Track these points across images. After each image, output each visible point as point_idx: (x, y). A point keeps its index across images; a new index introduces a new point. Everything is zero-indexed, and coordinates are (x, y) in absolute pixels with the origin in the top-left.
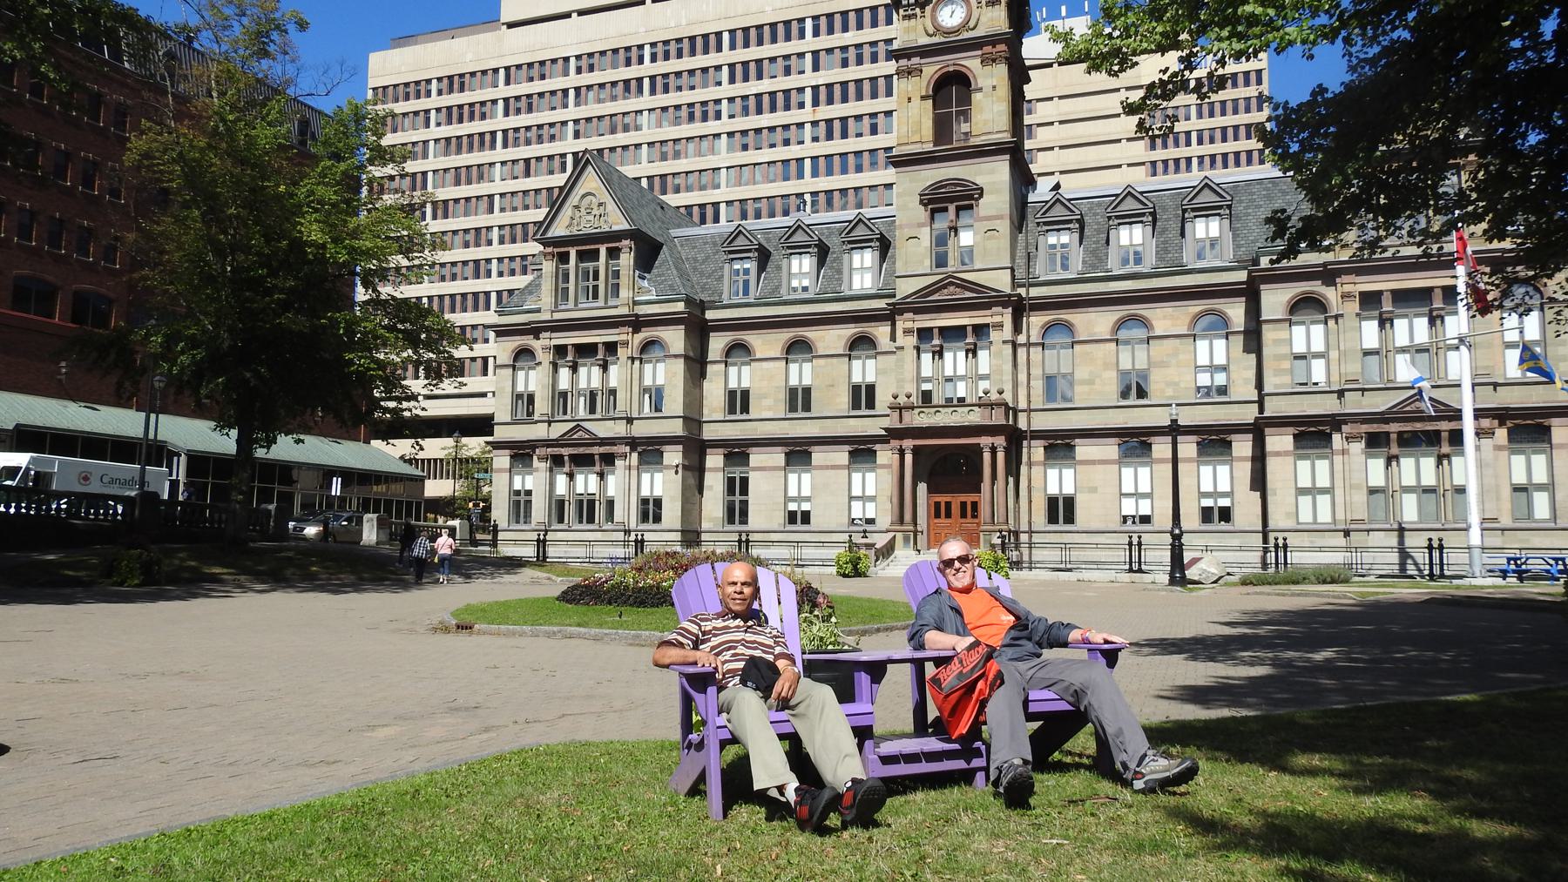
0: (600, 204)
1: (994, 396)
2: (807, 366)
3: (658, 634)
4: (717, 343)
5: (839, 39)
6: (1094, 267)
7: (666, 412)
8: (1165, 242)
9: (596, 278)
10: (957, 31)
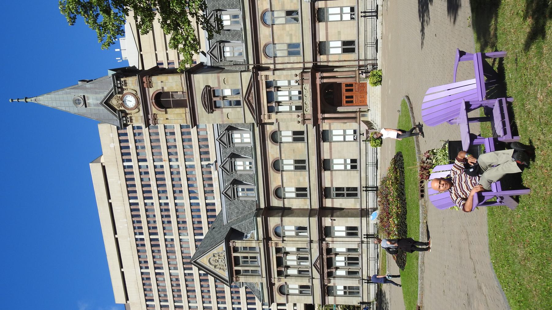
0: (214, 256)
1: (298, 78)
2: (285, 162)
3: (421, 225)
4: (275, 202)
5: (132, 150)
6: (240, 36)
7: (307, 225)
8: (229, 5)
9: (247, 257)
10: (137, 99)
